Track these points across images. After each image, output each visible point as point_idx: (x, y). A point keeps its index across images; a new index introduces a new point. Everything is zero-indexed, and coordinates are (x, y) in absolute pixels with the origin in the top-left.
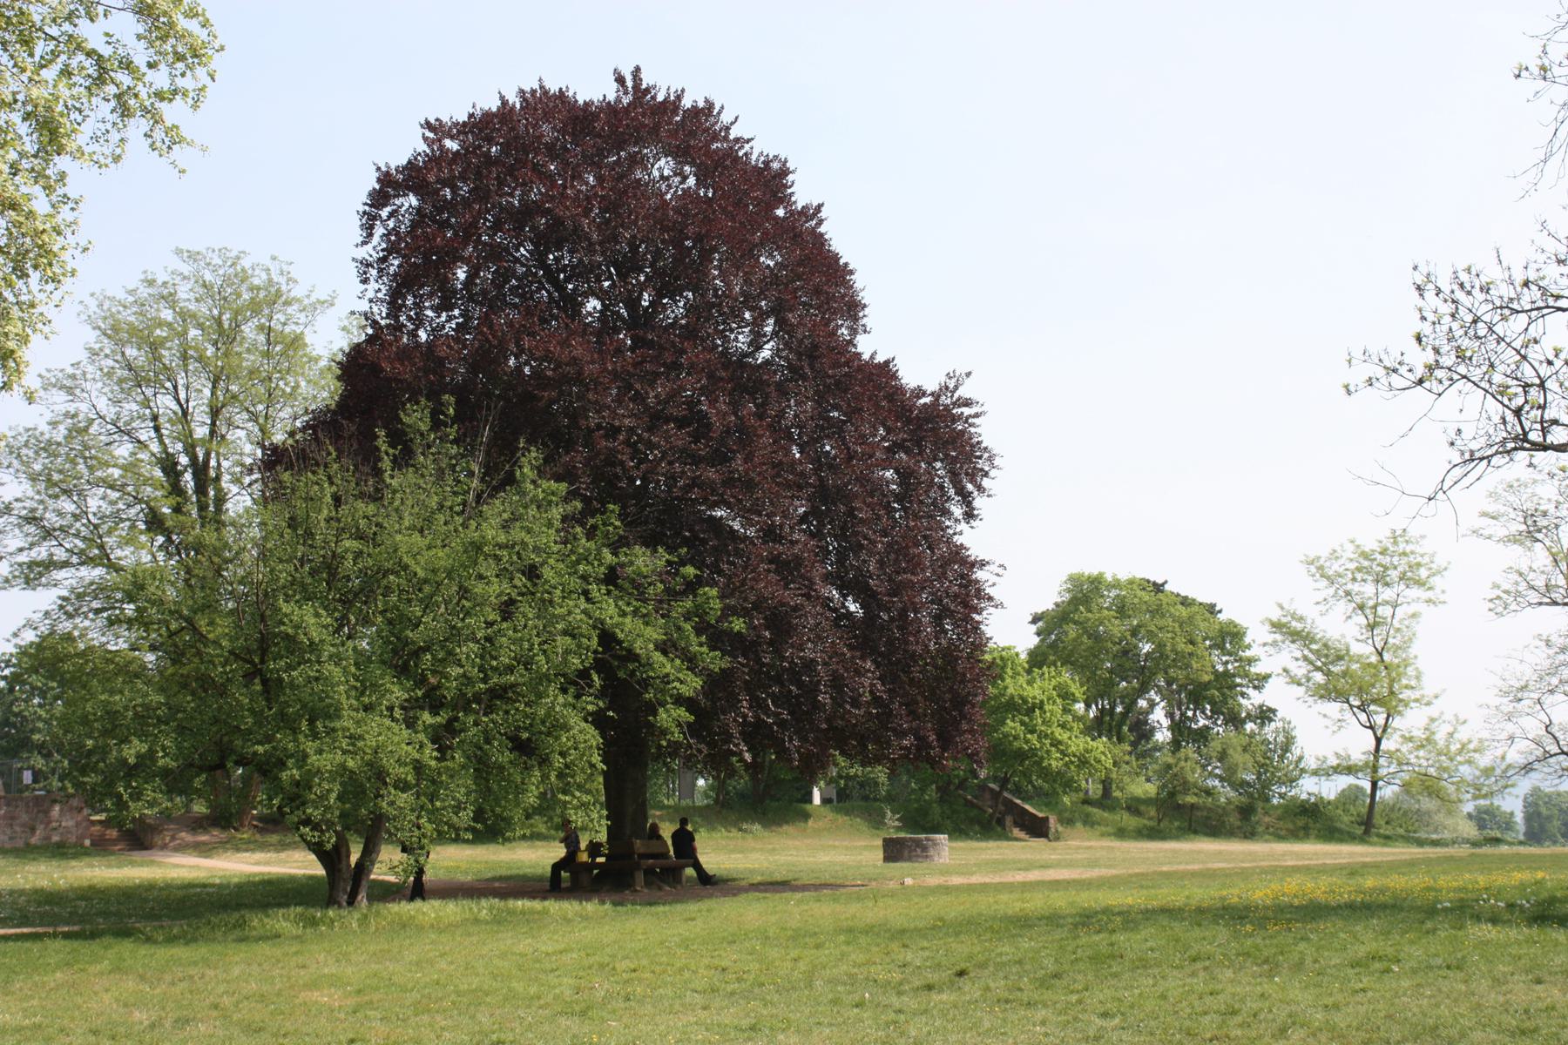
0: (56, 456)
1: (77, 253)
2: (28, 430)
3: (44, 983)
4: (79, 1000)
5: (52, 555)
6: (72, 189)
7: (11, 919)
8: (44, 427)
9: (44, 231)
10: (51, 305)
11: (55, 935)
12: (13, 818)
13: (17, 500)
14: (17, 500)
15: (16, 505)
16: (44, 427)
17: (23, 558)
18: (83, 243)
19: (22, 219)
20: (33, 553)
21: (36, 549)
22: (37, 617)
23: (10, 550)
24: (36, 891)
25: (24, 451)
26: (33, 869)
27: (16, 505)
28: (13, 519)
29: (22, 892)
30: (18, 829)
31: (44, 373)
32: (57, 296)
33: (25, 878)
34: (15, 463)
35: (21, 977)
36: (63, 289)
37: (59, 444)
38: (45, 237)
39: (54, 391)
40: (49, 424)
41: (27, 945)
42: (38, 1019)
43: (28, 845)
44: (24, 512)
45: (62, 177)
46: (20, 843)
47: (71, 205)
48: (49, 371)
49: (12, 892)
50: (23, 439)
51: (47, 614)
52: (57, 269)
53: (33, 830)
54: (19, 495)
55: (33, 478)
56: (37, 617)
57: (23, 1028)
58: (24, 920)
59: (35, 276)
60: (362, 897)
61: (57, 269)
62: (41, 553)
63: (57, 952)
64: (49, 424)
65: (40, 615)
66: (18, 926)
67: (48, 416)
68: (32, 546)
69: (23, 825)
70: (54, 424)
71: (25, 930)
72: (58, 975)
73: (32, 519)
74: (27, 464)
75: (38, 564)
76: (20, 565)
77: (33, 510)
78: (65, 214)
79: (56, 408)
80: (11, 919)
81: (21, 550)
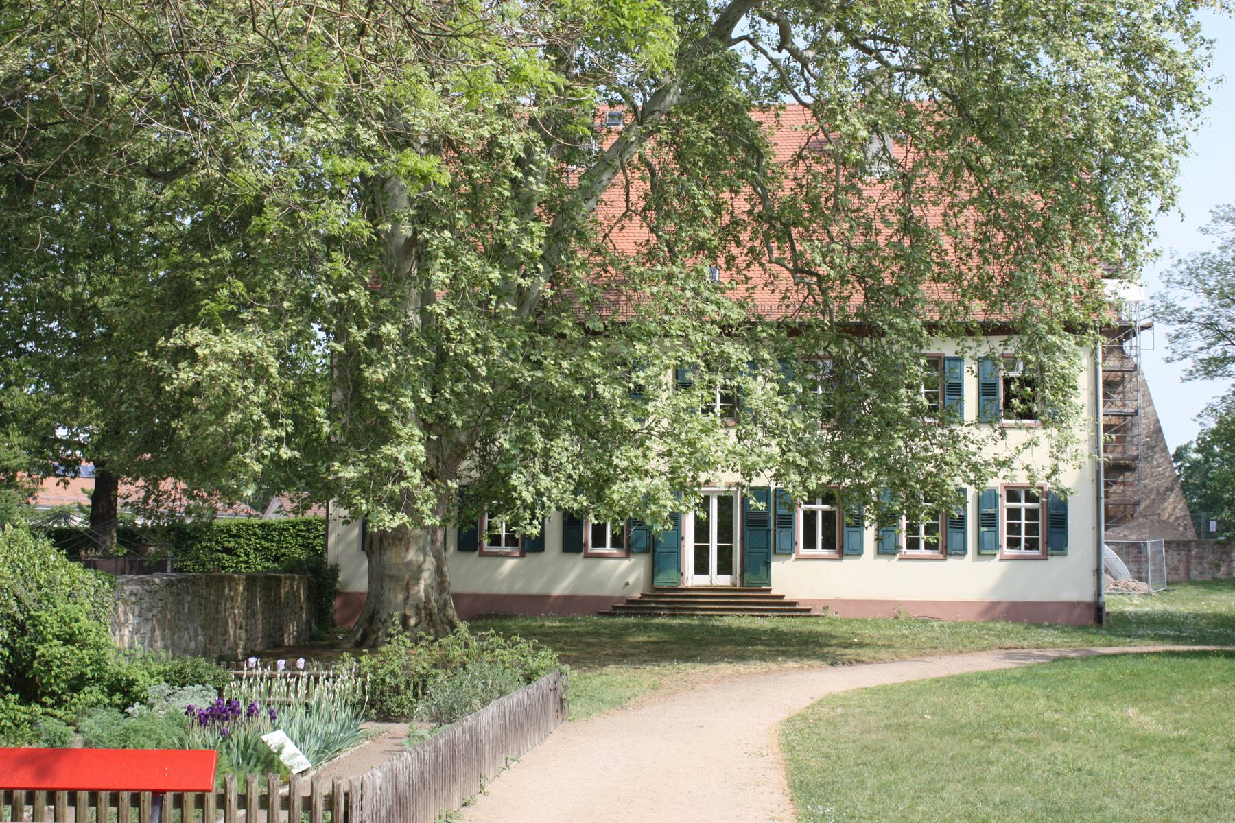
0: (1226, 274)
1: (1212, 84)
2: (1203, 254)
3: (1200, 696)
4: (1225, 716)
5: (1226, 352)
6: (1205, 33)
7: (1191, 638)
8: (1216, 252)
9: (1184, 66)
10: (1191, 129)
11: (1217, 654)
12: (1202, 558)
13: (1197, 310)
14: (1197, 310)
15: (1196, 314)
16: (1216, 252)
17: (1204, 355)
18: (1217, 76)
19: (1165, 58)
20: (1212, 351)
21: (1213, 348)
22: (1216, 401)
23: (1193, 349)
24: (1215, 616)
25: (1201, 272)
26: (1216, 597)
27: (1196, 314)
28: (1194, 325)
29: (1204, 616)
30: (1206, 566)
31: (1214, 209)
32: (1196, 122)
33: (1209, 605)
34: (1195, 282)
35: (1183, 690)
36: (1202, 115)
37: (1228, 264)
38: (1185, 72)
39: (1223, 222)
40: (1220, 248)
41: (1195, 661)
42: (1184, 732)
43: (1214, 579)
44: (1202, 320)
45: (1197, 27)
46: (1208, 577)
47: (1206, 45)
48: (1218, 207)
49: (1196, 616)
50: (1198, 263)
51: (1223, 398)
52: (1196, 100)
53: (1218, 567)
54: (1198, 306)
55: (1209, 293)
56: (1216, 401)
57: (1169, 740)
58: (1202, 640)
59: (1178, 107)
60: (1130, 365)
61: (1196, 100)
62: (1216, 351)
63: (1217, 669)
64: (1220, 248)
65: (1219, 400)
66: (1196, 644)
67: (1219, 243)
68: (1210, 345)
69: (1210, 563)
70: (1223, 249)
71: (1197, 648)
72: (1214, 690)
73: (1210, 325)
74: (1203, 282)
75: (1215, 359)
76: (1201, 360)
77: (1210, 318)
78: (1201, 52)
79: (1225, 236)
80: (1191, 638)
81: (1201, 349)
